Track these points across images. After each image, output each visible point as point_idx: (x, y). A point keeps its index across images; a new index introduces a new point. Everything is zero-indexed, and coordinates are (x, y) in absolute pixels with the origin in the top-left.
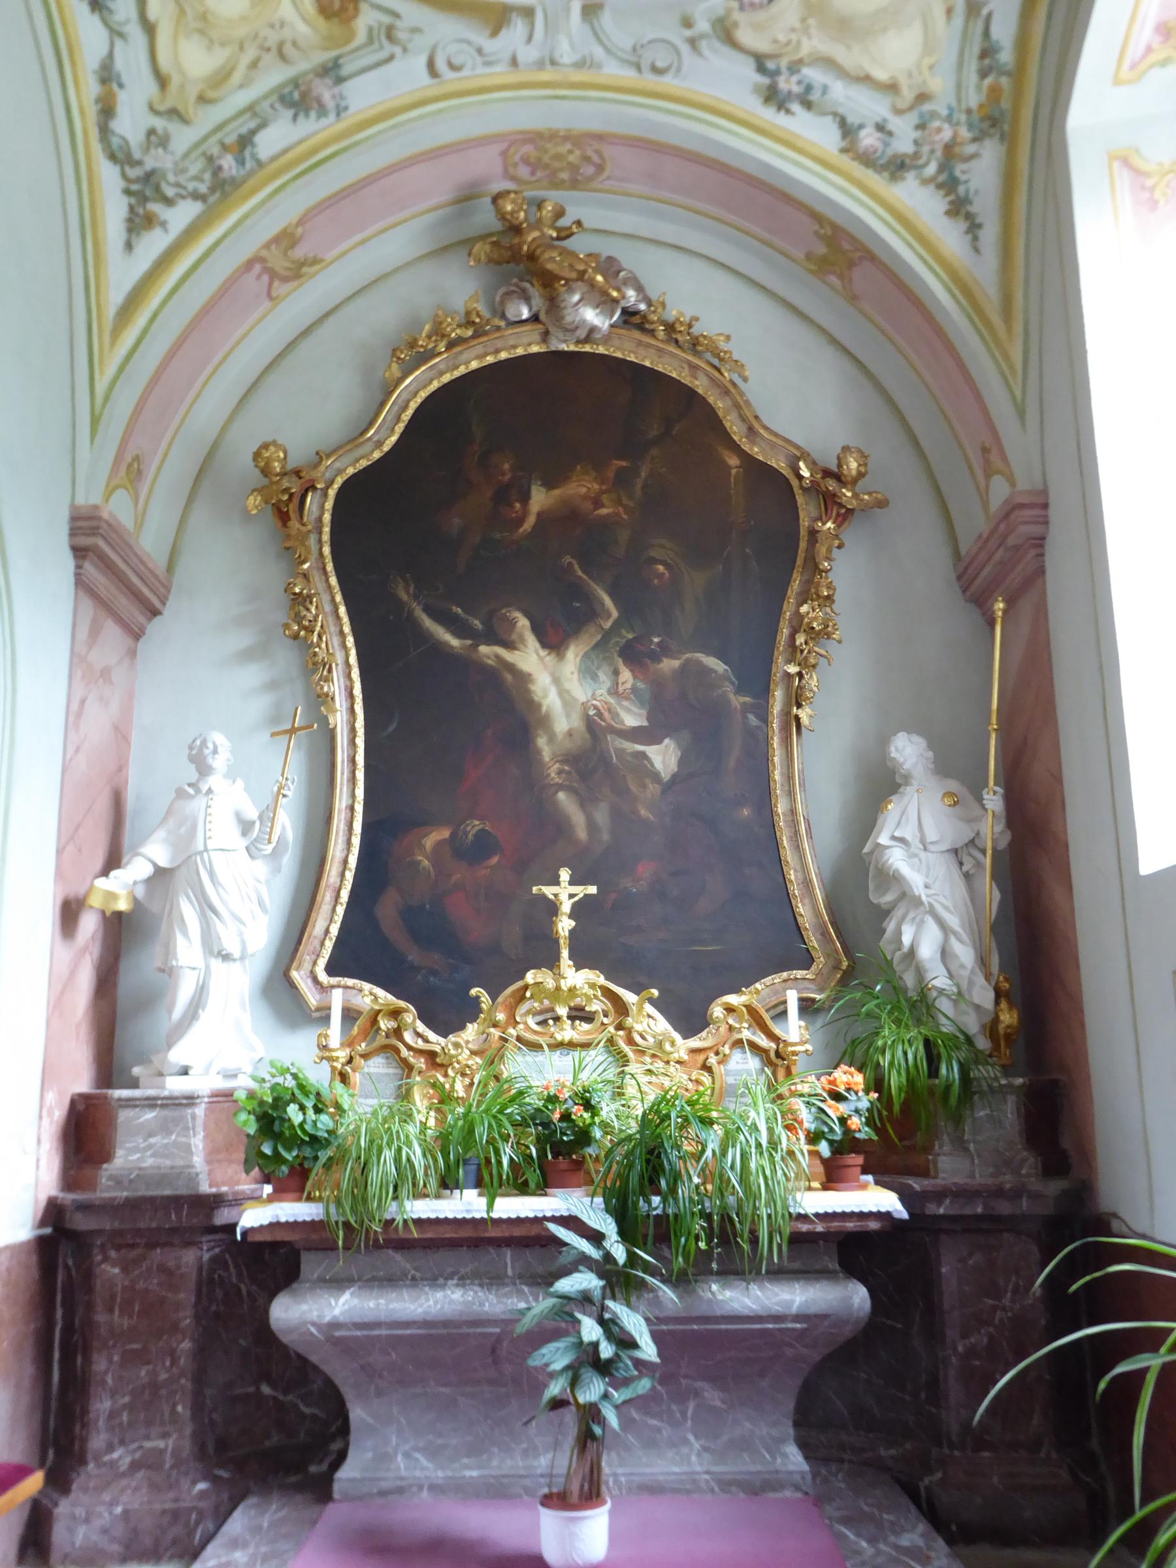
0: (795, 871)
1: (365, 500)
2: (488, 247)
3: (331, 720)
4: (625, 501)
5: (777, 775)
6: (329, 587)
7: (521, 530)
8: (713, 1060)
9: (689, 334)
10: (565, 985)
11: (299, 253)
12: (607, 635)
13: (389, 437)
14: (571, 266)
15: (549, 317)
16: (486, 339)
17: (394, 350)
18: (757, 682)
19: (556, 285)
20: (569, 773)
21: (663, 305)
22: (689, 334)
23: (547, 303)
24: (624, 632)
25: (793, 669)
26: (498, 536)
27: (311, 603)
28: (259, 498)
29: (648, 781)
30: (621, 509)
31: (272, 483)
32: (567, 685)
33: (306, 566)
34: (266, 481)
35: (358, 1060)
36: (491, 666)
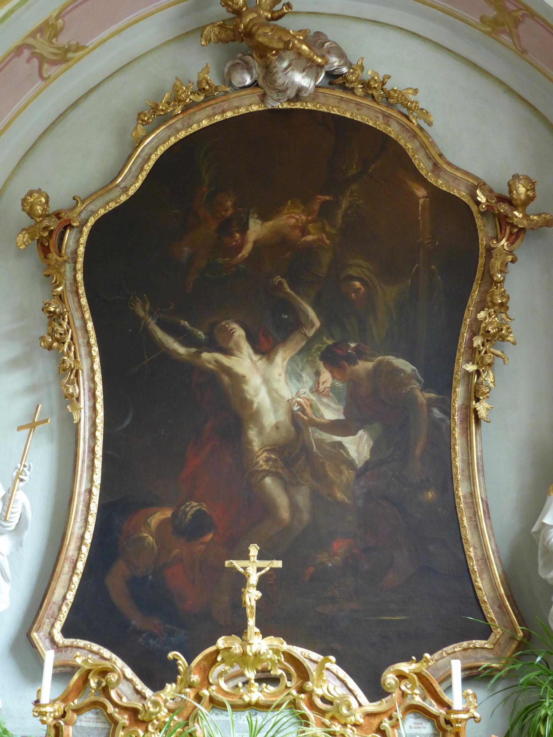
0: (475, 548)
1: (111, 234)
2: (216, 30)
3: (76, 418)
4: (328, 229)
5: (458, 462)
6: (81, 306)
7: (240, 256)
8: (386, 724)
9: (382, 89)
10: (250, 650)
11: (63, 40)
12: (310, 342)
13: (134, 183)
14: (280, 39)
15: (266, 83)
16: (214, 102)
17: (139, 114)
18: (440, 379)
19: (269, 55)
20: (275, 461)
21: (362, 68)
22: (382, 89)
23: (264, 70)
24: (325, 339)
25: (471, 368)
26: (220, 261)
27: (64, 319)
28: (27, 236)
29: (343, 467)
30: (324, 235)
31: (37, 223)
32: (275, 385)
33: (60, 289)
34: (32, 222)
35: (70, 715)
36: (211, 370)
